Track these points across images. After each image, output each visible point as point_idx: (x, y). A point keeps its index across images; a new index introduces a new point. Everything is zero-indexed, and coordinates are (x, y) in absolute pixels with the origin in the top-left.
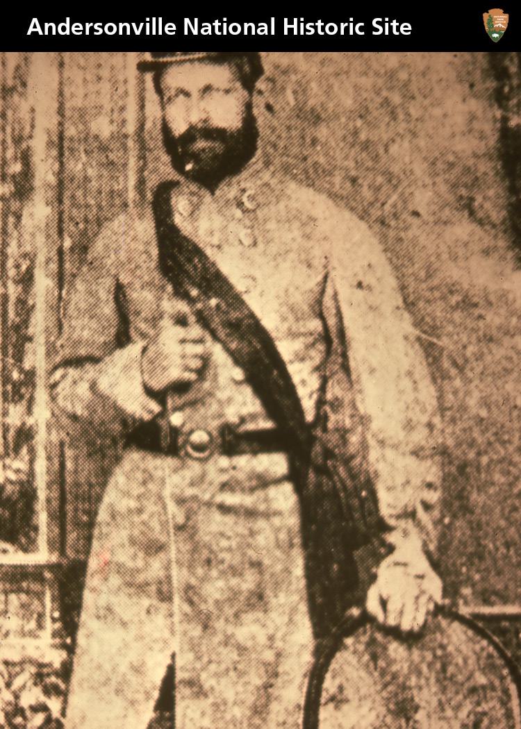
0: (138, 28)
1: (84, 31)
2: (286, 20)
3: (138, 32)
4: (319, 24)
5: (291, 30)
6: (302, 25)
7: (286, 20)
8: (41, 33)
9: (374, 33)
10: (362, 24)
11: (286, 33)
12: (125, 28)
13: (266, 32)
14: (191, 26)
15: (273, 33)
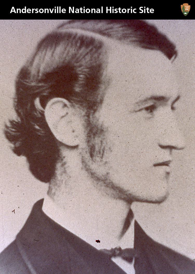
0: (52, 11)
1: (31, 12)
2: (107, 8)
3: (51, 12)
4: (120, 9)
5: (109, 11)
6: (113, 9)
7: (107, 8)
8: (15, 12)
9: (140, 12)
10: (136, 9)
11: (107, 12)
12: (47, 11)
13: (100, 12)
14: (71, 10)
15: (102, 12)
